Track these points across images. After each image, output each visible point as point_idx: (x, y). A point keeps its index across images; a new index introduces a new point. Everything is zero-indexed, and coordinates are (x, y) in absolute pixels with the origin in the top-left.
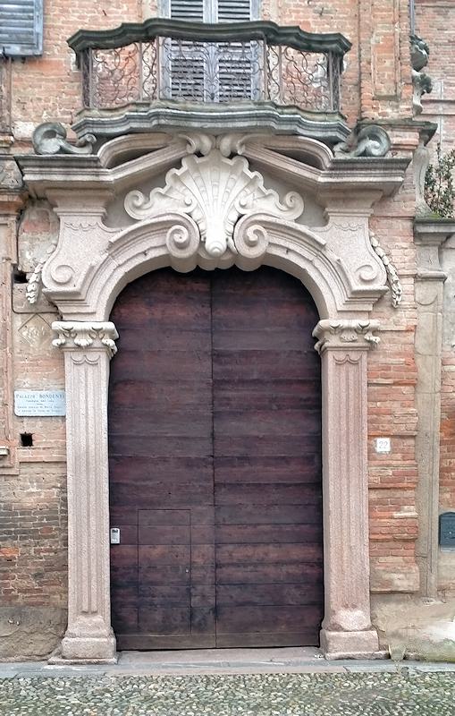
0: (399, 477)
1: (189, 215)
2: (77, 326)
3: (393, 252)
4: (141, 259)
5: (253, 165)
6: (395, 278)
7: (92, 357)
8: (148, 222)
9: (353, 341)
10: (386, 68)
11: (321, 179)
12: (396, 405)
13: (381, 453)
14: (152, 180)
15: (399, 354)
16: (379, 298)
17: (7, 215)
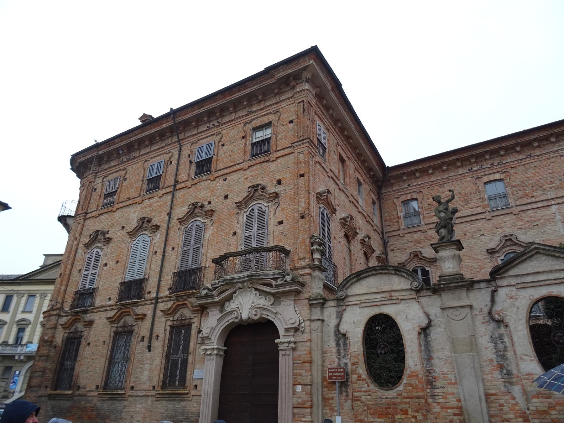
0: (304, 402)
1: (238, 308)
2: (207, 347)
3: (302, 312)
4: (228, 323)
5: (256, 289)
6: (302, 321)
7: (212, 357)
8: (230, 310)
9: (287, 347)
10: (303, 249)
12: (304, 371)
13: (298, 392)
14: (229, 298)
15: (305, 350)
16: (296, 330)
17: (198, 313)
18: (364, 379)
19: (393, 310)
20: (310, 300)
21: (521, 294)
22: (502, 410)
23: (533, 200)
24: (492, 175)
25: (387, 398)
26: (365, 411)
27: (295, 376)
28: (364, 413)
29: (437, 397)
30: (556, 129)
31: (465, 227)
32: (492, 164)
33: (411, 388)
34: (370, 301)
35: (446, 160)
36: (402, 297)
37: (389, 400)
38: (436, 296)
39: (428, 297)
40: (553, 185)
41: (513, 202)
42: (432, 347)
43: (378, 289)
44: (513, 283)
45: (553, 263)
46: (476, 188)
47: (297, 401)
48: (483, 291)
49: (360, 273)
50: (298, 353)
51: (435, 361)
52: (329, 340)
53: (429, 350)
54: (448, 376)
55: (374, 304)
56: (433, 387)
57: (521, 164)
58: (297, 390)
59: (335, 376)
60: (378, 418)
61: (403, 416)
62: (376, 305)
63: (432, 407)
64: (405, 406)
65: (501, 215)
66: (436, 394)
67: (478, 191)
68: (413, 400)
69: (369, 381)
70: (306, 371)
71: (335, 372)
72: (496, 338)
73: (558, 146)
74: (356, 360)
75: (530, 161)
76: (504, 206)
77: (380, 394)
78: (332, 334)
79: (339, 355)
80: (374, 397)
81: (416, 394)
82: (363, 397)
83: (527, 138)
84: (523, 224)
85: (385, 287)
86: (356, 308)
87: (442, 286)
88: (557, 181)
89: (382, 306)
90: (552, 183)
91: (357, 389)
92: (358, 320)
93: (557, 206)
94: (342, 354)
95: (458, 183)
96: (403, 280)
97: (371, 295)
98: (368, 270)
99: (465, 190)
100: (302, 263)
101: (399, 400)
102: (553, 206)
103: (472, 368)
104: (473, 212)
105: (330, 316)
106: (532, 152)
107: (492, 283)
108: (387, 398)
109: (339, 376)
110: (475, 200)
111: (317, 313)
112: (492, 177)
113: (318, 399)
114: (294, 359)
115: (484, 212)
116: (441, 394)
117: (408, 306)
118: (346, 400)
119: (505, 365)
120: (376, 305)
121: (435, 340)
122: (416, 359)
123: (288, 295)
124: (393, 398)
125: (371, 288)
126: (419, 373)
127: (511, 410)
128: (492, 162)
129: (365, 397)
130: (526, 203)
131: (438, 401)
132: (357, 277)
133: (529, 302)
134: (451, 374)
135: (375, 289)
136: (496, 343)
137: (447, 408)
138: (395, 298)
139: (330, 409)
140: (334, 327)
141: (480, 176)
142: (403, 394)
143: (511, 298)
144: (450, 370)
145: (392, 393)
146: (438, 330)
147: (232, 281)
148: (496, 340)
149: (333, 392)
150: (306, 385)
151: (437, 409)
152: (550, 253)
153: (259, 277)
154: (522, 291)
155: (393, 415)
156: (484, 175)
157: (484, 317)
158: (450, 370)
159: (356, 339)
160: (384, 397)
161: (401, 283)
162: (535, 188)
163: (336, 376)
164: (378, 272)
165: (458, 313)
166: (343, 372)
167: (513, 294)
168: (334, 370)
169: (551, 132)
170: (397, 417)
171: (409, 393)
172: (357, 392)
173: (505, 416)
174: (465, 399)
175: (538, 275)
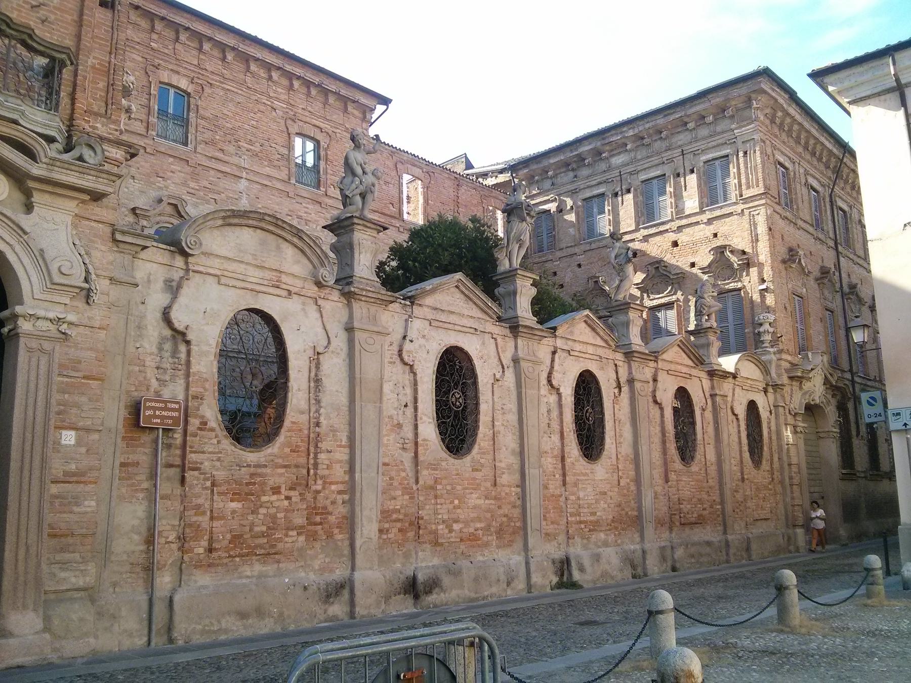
12: (84, 399)
18: (212, 430)
26: (206, 488)
27: (62, 408)
40: (251, 147)
43: (256, 259)
70: (90, 400)
75: (236, 90)
82: (206, 464)
84: (197, 188)
90: (251, 142)
116: (327, 462)
135: (250, 257)
142: (276, 461)
145: (251, 457)
155: (258, 497)
166: (178, 410)
168: (157, 405)
170: (264, 499)
172: (195, 452)
173: (393, 493)
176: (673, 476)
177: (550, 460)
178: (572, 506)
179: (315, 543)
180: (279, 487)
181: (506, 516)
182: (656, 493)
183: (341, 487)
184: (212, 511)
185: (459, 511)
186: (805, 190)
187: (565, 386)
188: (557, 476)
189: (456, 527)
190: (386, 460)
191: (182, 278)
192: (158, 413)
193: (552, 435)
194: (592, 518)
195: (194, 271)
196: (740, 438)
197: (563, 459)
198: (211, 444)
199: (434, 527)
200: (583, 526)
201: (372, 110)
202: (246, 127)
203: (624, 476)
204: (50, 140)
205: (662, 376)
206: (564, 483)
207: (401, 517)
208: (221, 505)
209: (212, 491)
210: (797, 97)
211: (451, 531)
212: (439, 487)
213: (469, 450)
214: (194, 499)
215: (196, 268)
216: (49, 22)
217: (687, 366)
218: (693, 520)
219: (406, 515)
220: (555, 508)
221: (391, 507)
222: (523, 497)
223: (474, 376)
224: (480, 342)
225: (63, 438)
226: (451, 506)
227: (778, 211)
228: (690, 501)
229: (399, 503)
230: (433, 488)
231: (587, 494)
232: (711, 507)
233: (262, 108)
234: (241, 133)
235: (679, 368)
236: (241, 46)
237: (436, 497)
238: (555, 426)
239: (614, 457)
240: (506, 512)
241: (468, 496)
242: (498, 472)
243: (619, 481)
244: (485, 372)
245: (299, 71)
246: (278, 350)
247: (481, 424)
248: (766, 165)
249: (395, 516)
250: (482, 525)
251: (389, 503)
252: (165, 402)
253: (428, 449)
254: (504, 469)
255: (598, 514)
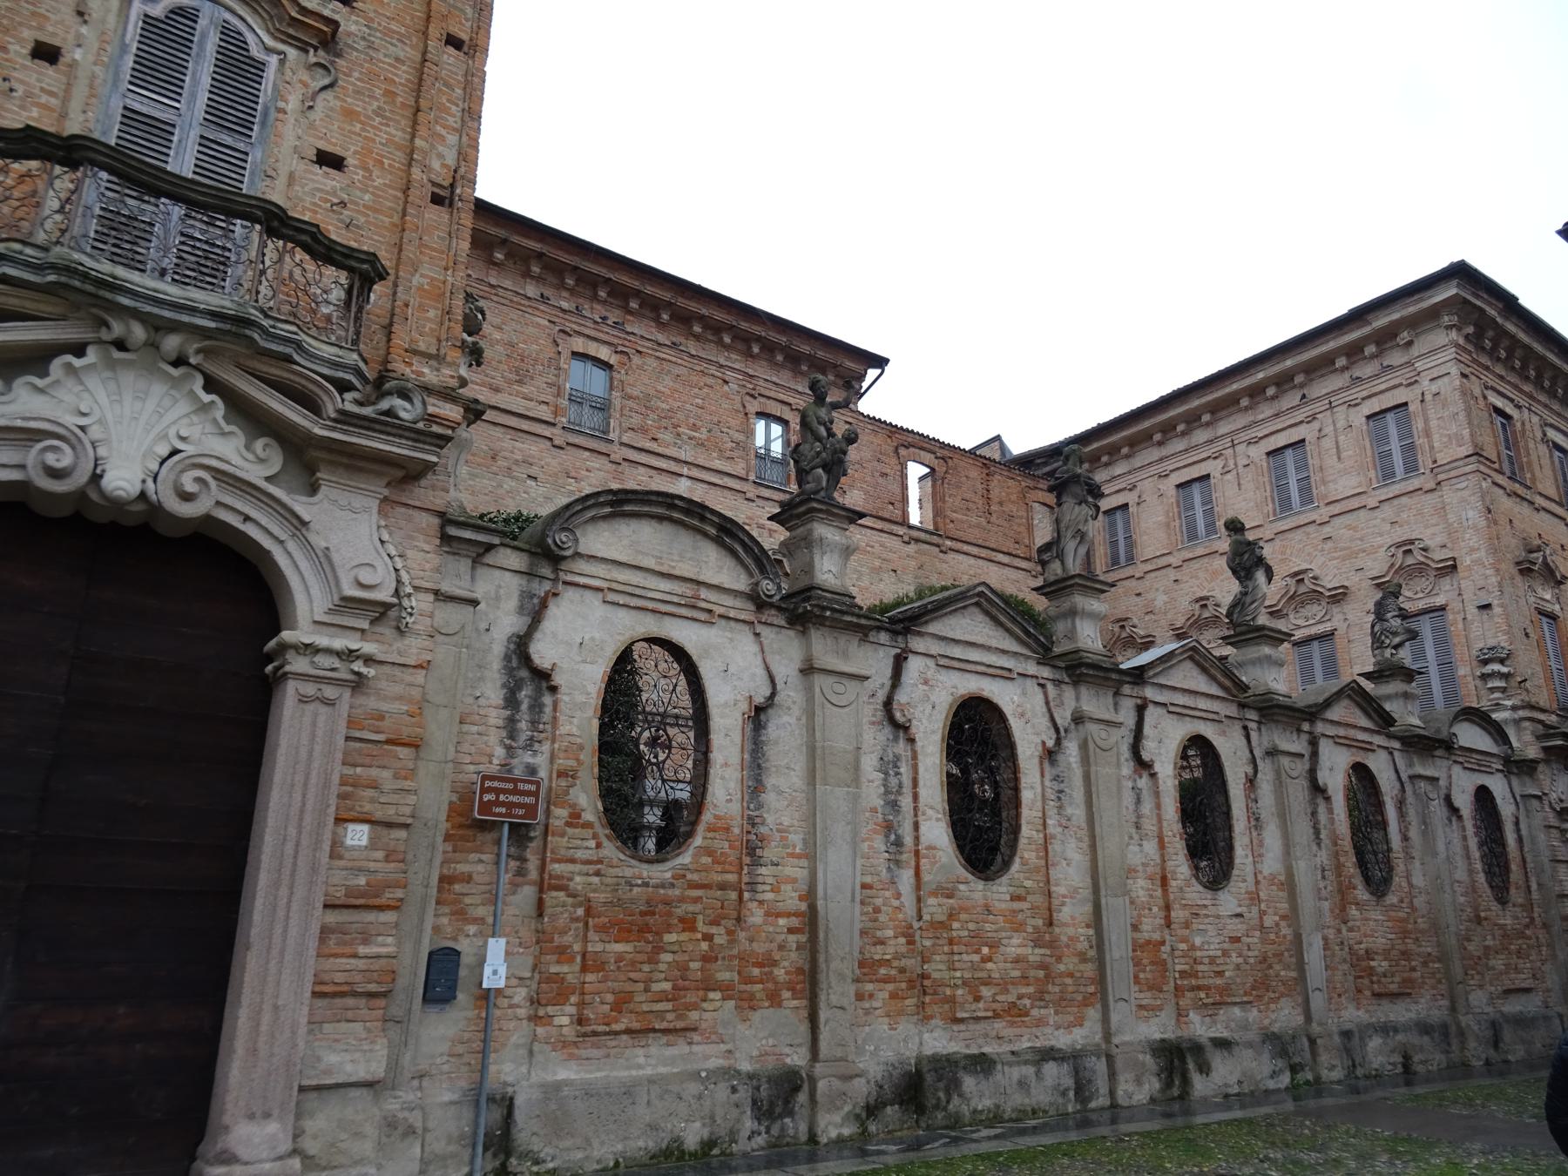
3: (409, 553)
5: (211, 385)
11: (318, 431)
12: (386, 774)
13: (353, 848)
15: (400, 698)
16: (381, 612)
18: (587, 825)
19: (694, 638)
20: (445, 519)
21: (941, 678)
22: (876, 920)
23: (649, 445)
24: (595, 344)
25: (646, 885)
26: (577, 920)
27: (349, 789)
28: (574, 926)
29: (761, 888)
30: (745, 321)
31: (499, 439)
32: (604, 318)
33: (710, 860)
34: (638, 591)
35: (516, 239)
36: (721, 610)
37: (650, 889)
38: (791, 633)
39: (775, 629)
41: (617, 432)
42: (767, 760)
44: (933, 652)
45: (991, 633)
46: (552, 355)
47: (340, 880)
48: (881, 652)
49: (630, 496)
50: (371, 703)
51: (769, 798)
52: (482, 679)
53: (759, 766)
54: (791, 836)
55: (650, 605)
56: (756, 862)
57: (657, 354)
58: (349, 842)
59: (503, 804)
60: (616, 942)
61: (685, 936)
62: (653, 611)
63: (748, 913)
64: (691, 908)
65: (586, 449)
66: (760, 879)
67: (554, 363)
68: (710, 893)
69: (603, 832)
70: (396, 777)
71: (505, 791)
72: (888, 763)
73: (727, 359)
74: (572, 763)
75: (674, 359)
76: (594, 429)
77: (628, 872)
78: (495, 664)
79: (512, 736)
80: (609, 881)
81: (718, 878)
82: (578, 879)
83: (693, 306)
85: (680, 564)
86: (594, 600)
87: (828, 613)
88: (704, 430)
89: (666, 617)
90: (695, 428)
91: (563, 852)
92: (593, 639)
93: (688, 483)
94: (523, 737)
95: (514, 314)
96: (729, 562)
97: (647, 575)
98: (654, 498)
99: (525, 342)
100: (426, 370)
101: (677, 892)
102: (683, 480)
103: (848, 824)
104: (528, 409)
105: (498, 598)
106: (683, 340)
107: (900, 639)
108: (646, 885)
109: (520, 806)
110: (540, 382)
111: (457, 577)
112: (594, 349)
113: (425, 873)
114: (351, 723)
115: (554, 425)
116: (770, 880)
117: (731, 640)
118: (517, 885)
119: (895, 824)
120: (653, 611)
121: (776, 743)
122: (732, 785)
123: (361, 470)
124: (663, 886)
125: (642, 553)
126: (734, 823)
127: (890, 920)
128: (605, 313)
129: (585, 878)
130: (639, 446)
131: (760, 897)
132: (611, 504)
133: (950, 699)
134: (796, 833)
135: (653, 561)
136: (886, 774)
137: (778, 915)
138: (704, 605)
139: (453, 914)
140: (505, 638)
141: (568, 330)
142: (689, 876)
143: (926, 682)
144: (796, 823)
146: (786, 719)
147: (108, 295)
148: (888, 766)
149: (474, 857)
150: (390, 825)
151: (756, 916)
152: (994, 611)
153: (274, 347)
154: (943, 671)
156: (579, 333)
157: (876, 710)
158: (796, 823)
159: (580, 698)
160: (640, 882)
161: (721, 568)
162: (664, 423)
163: (510, 805)
164: (676, 515)
165: (840, 688)
167: (930, 674)
168: (502, 785)
169: (734, 323)
170: (670, 938)
171: (704, 874)
172: (559, 861)
173: (879, 934)
174: (825, 894)
175: (971, 649)
176: (1354, 912)
177: (1141, 882)
178: (1183, 961)
179: (751, 1014)
180: (695, 920)
181: (1071, 975)
182: (1325, 939)
183: (795, 922)
184: (584, 956)
185: (990, 965)
186: (1543, 449)
187: (1163, 762)
188: (1155, 909)
189: (986, 992)
190: (868, 879)
191: (547, 593)
192: (502, 798)
193: (1145, 843)
194: (1219, 981)
195: (566, 583)
196: (1466, 848)
197: (1164, 881)
198: (587, 848)
199: (948, 992)
200: (1202, 995)
201: (862, 377)
202: (688, 406)
203: (1270, 911)
204: (343, 387)
205: (1325, 747)
206: (1168, 923)
207: (893, 972)
208: (599, 947)
209: (586, 924)
210: (1519, 305)
211: (977, 999)
212: (956, 925)
213: (1007, 864)
214: (556, 936)
215: (569, 578)
216: (357, 227)
217: (1365, 729)
218: (1394, 987)
219: (902, 970)
220: (1152, 963)
221: (877, 957)
222: (1100, 943)
223: (1011, 746)
224: (1019, 691)
225: (350, 835)
226: (976, 958)
227: (1500, 482)
228: (1386, 954)
229: (891, 950)
230: (943, 925)
231: (1208, 940)
232: (1425, 964)
233: (710, 381)
234: (680, 415)
235: (1352, 733)
236: (680, 299)
237: (951, 942)
238: (1149, 825)
239: (1251, 879)
240: (1071, 967)
241: (1004, 942)
242: (1055, 902)
243: (1261, 918)
244: (1028, 737)
245: (758, 330)
246: (694, 702)
247: (1023, 822)
248: (1474, 413)
249: (883, 971)
250: (1031, 990)
251: (873, 949)
252: (515, 781)
253: (936, 863)
254: (1064, 896)
255: (1227, 974)
